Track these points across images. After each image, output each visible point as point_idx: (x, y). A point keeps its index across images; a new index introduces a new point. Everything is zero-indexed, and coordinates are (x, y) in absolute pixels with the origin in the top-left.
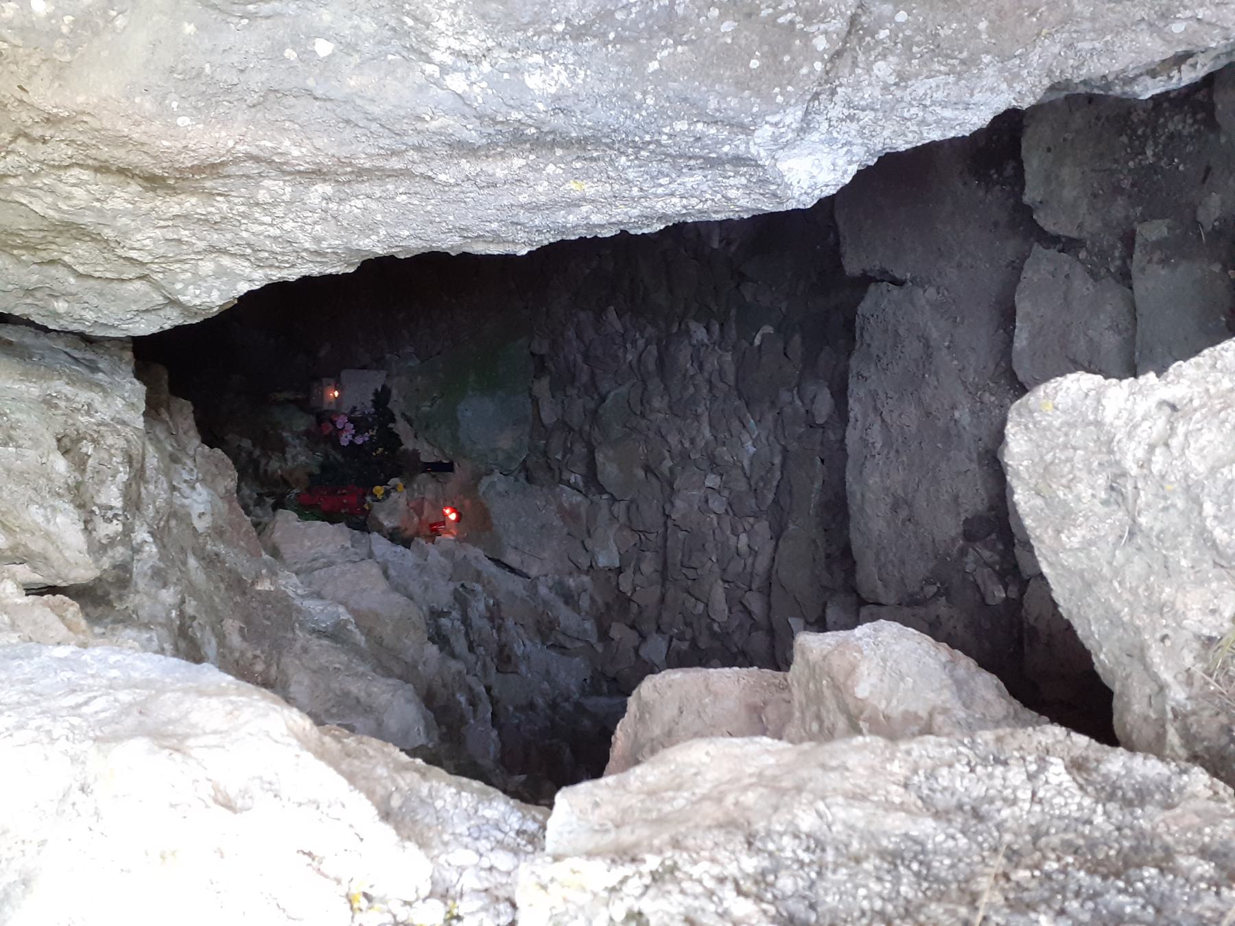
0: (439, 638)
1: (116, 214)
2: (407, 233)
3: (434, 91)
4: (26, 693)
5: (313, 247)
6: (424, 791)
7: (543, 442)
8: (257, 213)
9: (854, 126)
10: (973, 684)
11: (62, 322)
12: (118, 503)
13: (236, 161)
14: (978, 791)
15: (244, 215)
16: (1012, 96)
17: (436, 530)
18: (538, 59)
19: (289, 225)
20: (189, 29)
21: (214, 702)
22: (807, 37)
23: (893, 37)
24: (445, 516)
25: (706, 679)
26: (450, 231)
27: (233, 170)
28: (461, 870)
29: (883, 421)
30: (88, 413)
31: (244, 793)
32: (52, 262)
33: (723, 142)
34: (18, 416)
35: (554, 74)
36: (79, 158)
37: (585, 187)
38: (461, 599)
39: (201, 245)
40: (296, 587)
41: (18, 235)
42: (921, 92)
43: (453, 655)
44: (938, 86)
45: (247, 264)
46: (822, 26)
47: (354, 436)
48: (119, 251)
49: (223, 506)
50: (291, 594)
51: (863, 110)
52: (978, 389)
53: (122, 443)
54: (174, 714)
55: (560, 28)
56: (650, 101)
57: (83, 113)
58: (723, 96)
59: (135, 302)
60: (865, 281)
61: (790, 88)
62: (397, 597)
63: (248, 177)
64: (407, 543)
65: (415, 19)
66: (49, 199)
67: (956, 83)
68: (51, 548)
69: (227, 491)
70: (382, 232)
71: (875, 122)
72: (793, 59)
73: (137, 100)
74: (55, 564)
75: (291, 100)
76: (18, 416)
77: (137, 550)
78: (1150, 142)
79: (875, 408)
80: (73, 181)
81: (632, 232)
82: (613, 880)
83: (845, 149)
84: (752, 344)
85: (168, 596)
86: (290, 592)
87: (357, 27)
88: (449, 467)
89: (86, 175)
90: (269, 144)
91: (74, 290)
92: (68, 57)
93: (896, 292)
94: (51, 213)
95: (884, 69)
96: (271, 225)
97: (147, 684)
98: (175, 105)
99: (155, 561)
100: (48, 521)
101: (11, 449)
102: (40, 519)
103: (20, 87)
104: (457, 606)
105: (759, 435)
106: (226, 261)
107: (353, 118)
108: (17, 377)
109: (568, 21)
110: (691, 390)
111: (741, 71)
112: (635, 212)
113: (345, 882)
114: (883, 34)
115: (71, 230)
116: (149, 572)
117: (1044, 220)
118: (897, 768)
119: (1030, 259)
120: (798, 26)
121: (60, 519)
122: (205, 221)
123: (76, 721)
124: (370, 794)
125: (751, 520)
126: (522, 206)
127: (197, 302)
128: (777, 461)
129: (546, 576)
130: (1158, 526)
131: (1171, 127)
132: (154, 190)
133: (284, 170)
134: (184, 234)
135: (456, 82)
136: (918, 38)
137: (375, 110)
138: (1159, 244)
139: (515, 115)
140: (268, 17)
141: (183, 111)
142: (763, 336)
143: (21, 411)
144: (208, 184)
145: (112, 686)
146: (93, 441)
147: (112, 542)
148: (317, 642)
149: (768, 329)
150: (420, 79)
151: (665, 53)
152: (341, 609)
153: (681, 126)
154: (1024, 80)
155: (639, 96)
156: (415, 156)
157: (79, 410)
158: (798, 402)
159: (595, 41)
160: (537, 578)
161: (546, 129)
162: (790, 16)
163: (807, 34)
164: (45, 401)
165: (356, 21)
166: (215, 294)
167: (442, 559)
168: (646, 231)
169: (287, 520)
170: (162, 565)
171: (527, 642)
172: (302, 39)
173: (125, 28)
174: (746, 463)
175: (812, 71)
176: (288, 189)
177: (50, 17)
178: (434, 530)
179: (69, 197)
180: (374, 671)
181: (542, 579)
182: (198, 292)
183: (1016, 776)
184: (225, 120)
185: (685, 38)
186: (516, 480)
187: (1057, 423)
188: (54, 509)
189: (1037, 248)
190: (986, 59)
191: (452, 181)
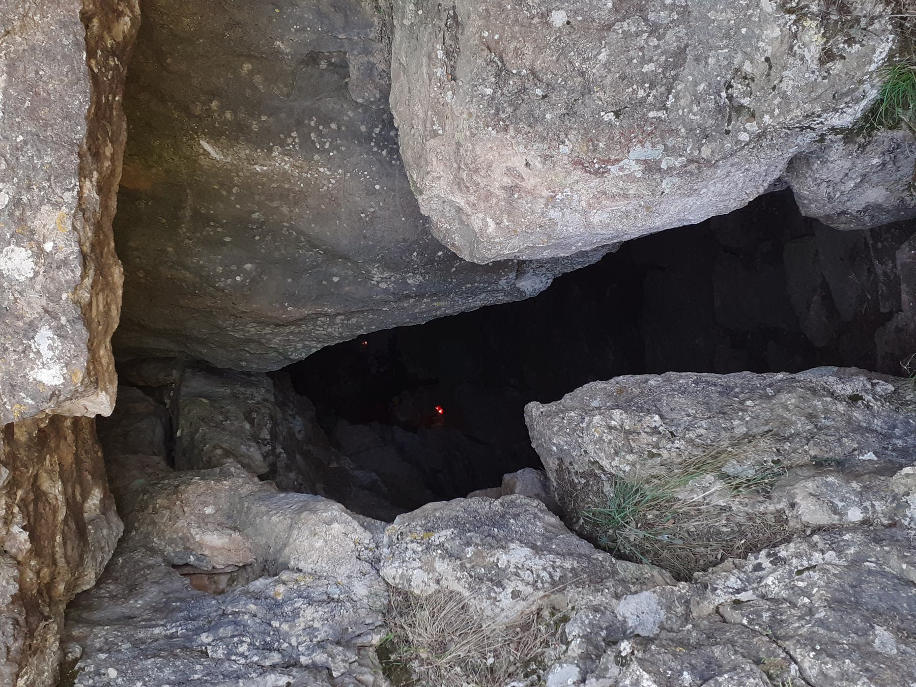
12: (268, 437)
19: (329, 330)
20: (290, 280)
24: (437, 411)
30: (252, 399)
32: (241, 350)
33: (487, 287)
34: (228, 407)
39: (297, 339)
50: (348, 468)
53: (268, 411)
56: (454, 281)
59: (272, 360)
70: (365, 328)
76: (228, 407)
77: (278, 456)
85: (292, 475)
102: (245, 450)
115: (249, 341)
133: (325, 315)
135: (383, 285)
139: (405, 292)
141: (289, 306)
143: (229, 405)
146: (256, 412)
152: (373, 474)
166: (303, 354)
177: (242, 281)
179: (249, 332)
188: (250, 446)
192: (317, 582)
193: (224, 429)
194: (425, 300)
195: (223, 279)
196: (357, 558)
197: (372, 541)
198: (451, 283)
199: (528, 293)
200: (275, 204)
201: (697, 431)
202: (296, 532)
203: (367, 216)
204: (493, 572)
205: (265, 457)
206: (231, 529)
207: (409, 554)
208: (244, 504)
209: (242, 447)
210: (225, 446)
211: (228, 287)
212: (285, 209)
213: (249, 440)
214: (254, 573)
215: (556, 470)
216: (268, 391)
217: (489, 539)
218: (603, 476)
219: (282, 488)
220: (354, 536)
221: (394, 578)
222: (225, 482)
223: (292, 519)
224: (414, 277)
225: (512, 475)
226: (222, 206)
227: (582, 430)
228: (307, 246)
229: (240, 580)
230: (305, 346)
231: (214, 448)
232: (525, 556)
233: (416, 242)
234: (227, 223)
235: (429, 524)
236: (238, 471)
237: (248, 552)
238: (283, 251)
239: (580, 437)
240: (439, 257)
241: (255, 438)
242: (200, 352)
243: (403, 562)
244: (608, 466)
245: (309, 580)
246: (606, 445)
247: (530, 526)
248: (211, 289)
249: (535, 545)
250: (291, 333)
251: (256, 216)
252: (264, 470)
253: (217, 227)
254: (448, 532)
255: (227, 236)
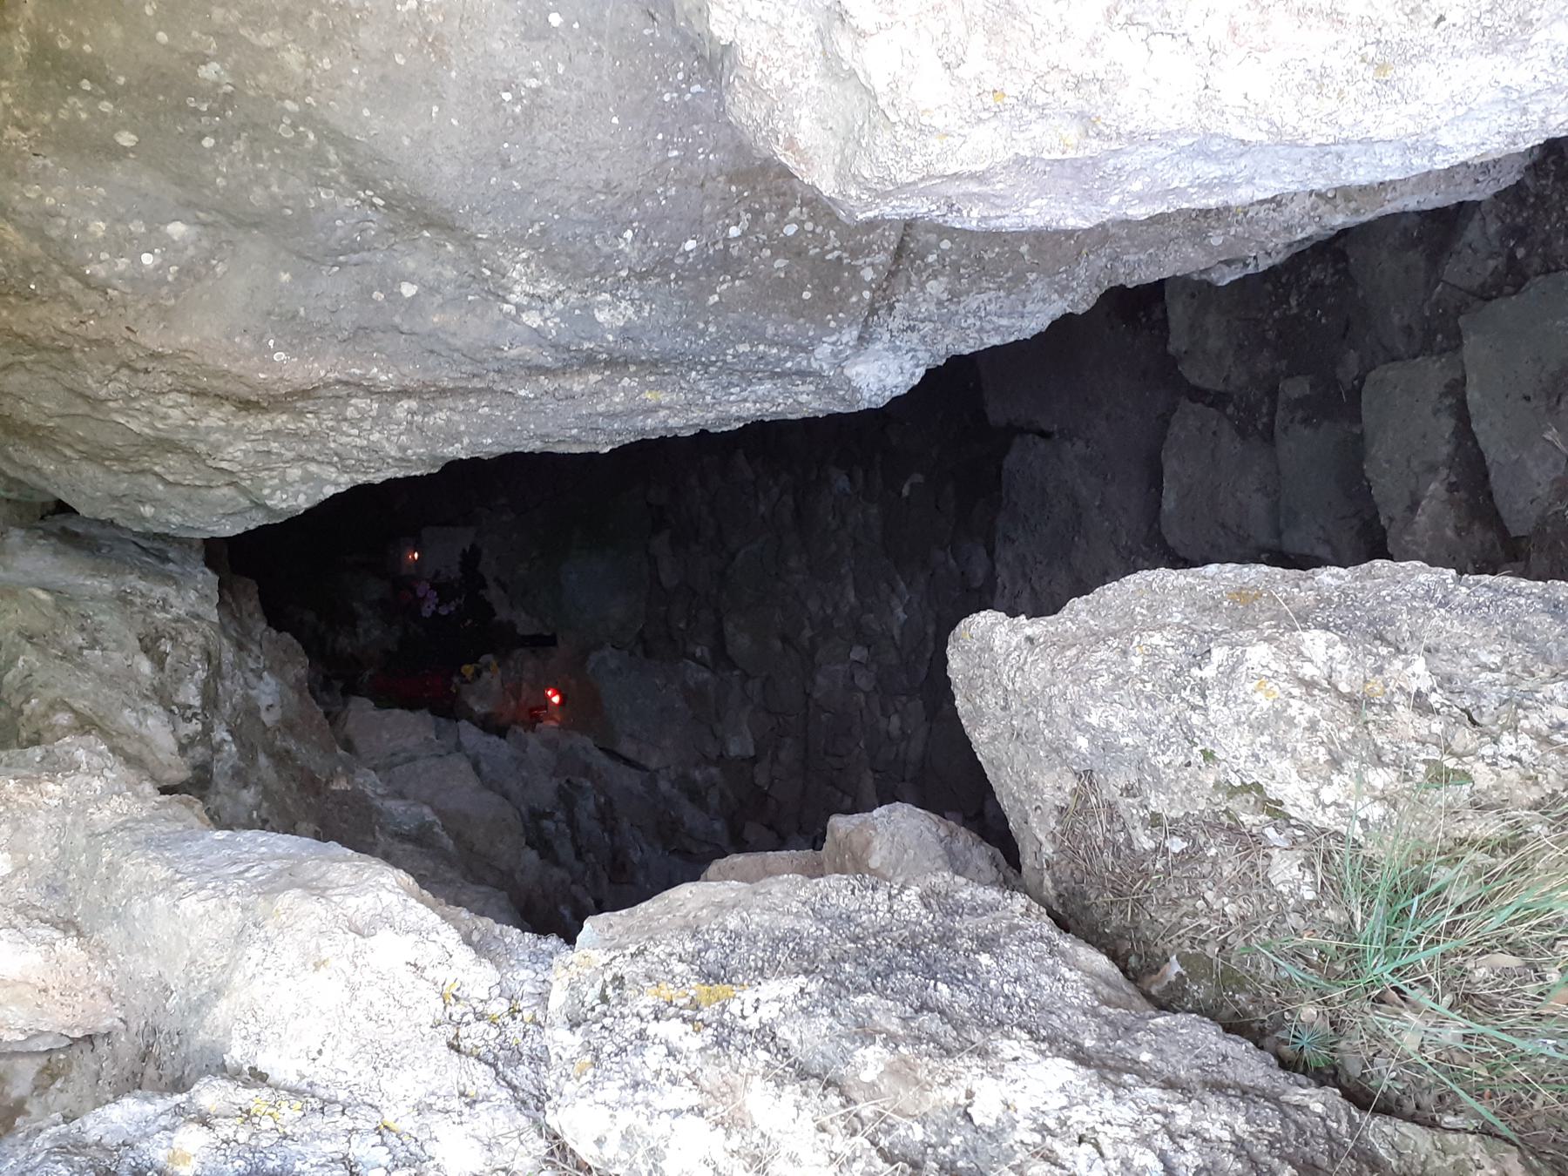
0: (541, 844)
1: (209, 430)
2: (490, 441)
3: (511, 325)
4: (199, 865)
5: (399, 455)
6: (497, 932)
7: (664, 608)
8: (345, 427)
9: (915, 337)
10: (969, 855)
11: (147, 525)
13: (327, 385)
14: (854, 906)
15: (332, 429)
16: (1065, 305)
17: (537, 716)
18: (606, 296)
19: (375, 437)
20: (285, 277)
21: (344, 866)
22: (855, 271)
23: (941, 259)
25: (764, 862)
26: (531, 437)
27: (323, 392)
28: (522, 982)
29: (1032, 588)
30: (163, 609)
31: (368, 925)
32: (143, 472)
33: (786, 360)
35: (621, 309)
36: (178, 385)
37: (660, 396)
38: (567, 798)
39: (290, 455)
40: (376, 785)
41: (112, 450)
42: (974, 306)
43: (557, 863)
44: (990, 300)
45: (333, 469)
46: (868, 260)
47: (437, 606)
48: (210, 462)
49: (293, 697)
51: (922, 322)
52: (1131, 553)
53: (201, 640)
54: (315, 875)
55: (624, 273)
56: (712, 329)
57: (186, 351)
58: (779, 324)
59: (222, 506)
60: (1013, 431)
61: (841, 315)
62: (488, 795)
63: (338, 397)
64: (502, 732)
65: (491, 270)
66: (146, 419)
67: (1008, 296)
68: (145, 752)
69: (297, 680)
70: (466, 441)
71: (936, 330)
72: (842, 290)
73: (237, 340)
74: (150, 766)
75: (379, 335)
77: (217, 749)
78: (1294, 291)
79: (1024, 575)
80: (170, 403)
81: (712, 431)
82: (606, 960)
83: (910, 354)
84: (900, 494)
86: (369, 791)
87: (440, 274)
88: (551, 641)
89: (182, 399)
90: (358, 372)
91: (162, 496)
92: (172, 302)
93: (1042, 445)
94: (147, 430)
95: (935, 287)
96: (359, 436)
97: (289, 856)
98: (271, 343)
99: (235, 760)
100: (141, 724)
101: (98, 652)
102: (133, 723)
103: (128, 328)
104: (562, 805)
105: (910, 600)
106: (313, 468)
107: (436, 348)
108: (88, 572)
109: (630, 269)
110: (833, 547)
111: (794, 301)
112: (712, 415)
113: (440, 984)
114: (931, 258)
115: (166, 445)
116: (230, 773)
117: (1193, 374)
118: (803, 894)
119: (1177, 414)
120: (845, 261)
121: (150, 722)
122: (295, 434)
123: (241, 882)
124: (458, 929)
125: (904, 699)
126: (600, 414)
127: (284, 506)
128: (931, 630)
129: (668, 767)
130: (1025, 727)
131: (1314, 275)
132: (247, 410)
133: (371, 391)
134: (274, 446)
135: (532, 319)
136: (964, 262)
137: (458, 343)
138: (1300, 403)
139: (586, 345)
140: (356, 265)
141: (278, 348)
142: (912, 486)
143: (103, 612)
144: (299, 404)
145: (262, 859)
147: (192, 741)
148: (400, 846)
149: (918, 478)
150: (498, 317)
151: (725, 286)
152: (426, 810)
153: (743, 348)
154: (1073, 290)
155: (701, 325)
156: (497, 377)
157: (154, 606)
158: (952, 561)
159: (659, 280)
160: (657, 771)
161: (616, 355)
162: (836, 253)
163: (855, 266)
164: (119, 598)
165: (438, 268)
166: (302, 498)
167: (544, 750)
168: (725, 429)
169: (361, 710)
170: (242, 765)
171: (645, 846)
172: (389, 284)
173: (225, 273)
174: (896, 632)
175: (861, 299)
176: (375, 406)
177: (157, 268)
178: (535, 714)
179: (165, 417)
180: (465, 877)
181: (663, 772)
182: (284, 496)
183: (881, 896)
184: (317, 355)
185: (741, 275)
186: (632, 653)
187: (974, 648)
189: (1185, 405)
190: (1032, 276)
191: (531, 396)
192: (317, 1121)
193: (84, 667)
194: (626, 381)
195: (104, 256)
196: (451, 1046)
197: (496, 991)
198: (703, 334)
199: (867, 395)
200: (267, 39)
201: (1547, 713)
202: (255, 952)
203: (518, 99)
204: (956, 1140)
205: (183, 749)
206: (55, 926)
207: (654, 1056)
208: (98, 855)
209: (127, 712)
210: (79, 705)
211: (118, 283)
212: (293, 58)
213: (147, 697)
214: (115, 1061)
215: (1062, 810)
216: (205, 598)
217: (930, 1022)
218: (1271, 832)
219: (218, 820)
220: (441, 974)
221: (599, 1142)
222: (51, 787)
223: (245, 909)
224: (613, 305)
225: (856, 819)
226: (116, 32)
227: (1202, 689)
228: (343, 179)
229: (74, 1074)
230: (307, 478)
231: (53, 707)
232: (1062, 1089)
233: (637, 197)
234: (127, 88)
235: (711, 955)
236: (96, 761)
237: (101, 1000)
238: (275, 189)
239: (1194, 708)
240: (686, 254)
241: (163, 696)
242: (38, 470)
243: (636, 1085)
244: (1306, 802)
245: (289, 1112)
246: (1297, 733)
247: (1044, 979)
248: (72, 282)
249: (1080, 1048)
250: (277, 433)
251: (209, 72)
252: (179, 772)
253: (102, 98)
254: (789, 987)
255: (124, 126)
